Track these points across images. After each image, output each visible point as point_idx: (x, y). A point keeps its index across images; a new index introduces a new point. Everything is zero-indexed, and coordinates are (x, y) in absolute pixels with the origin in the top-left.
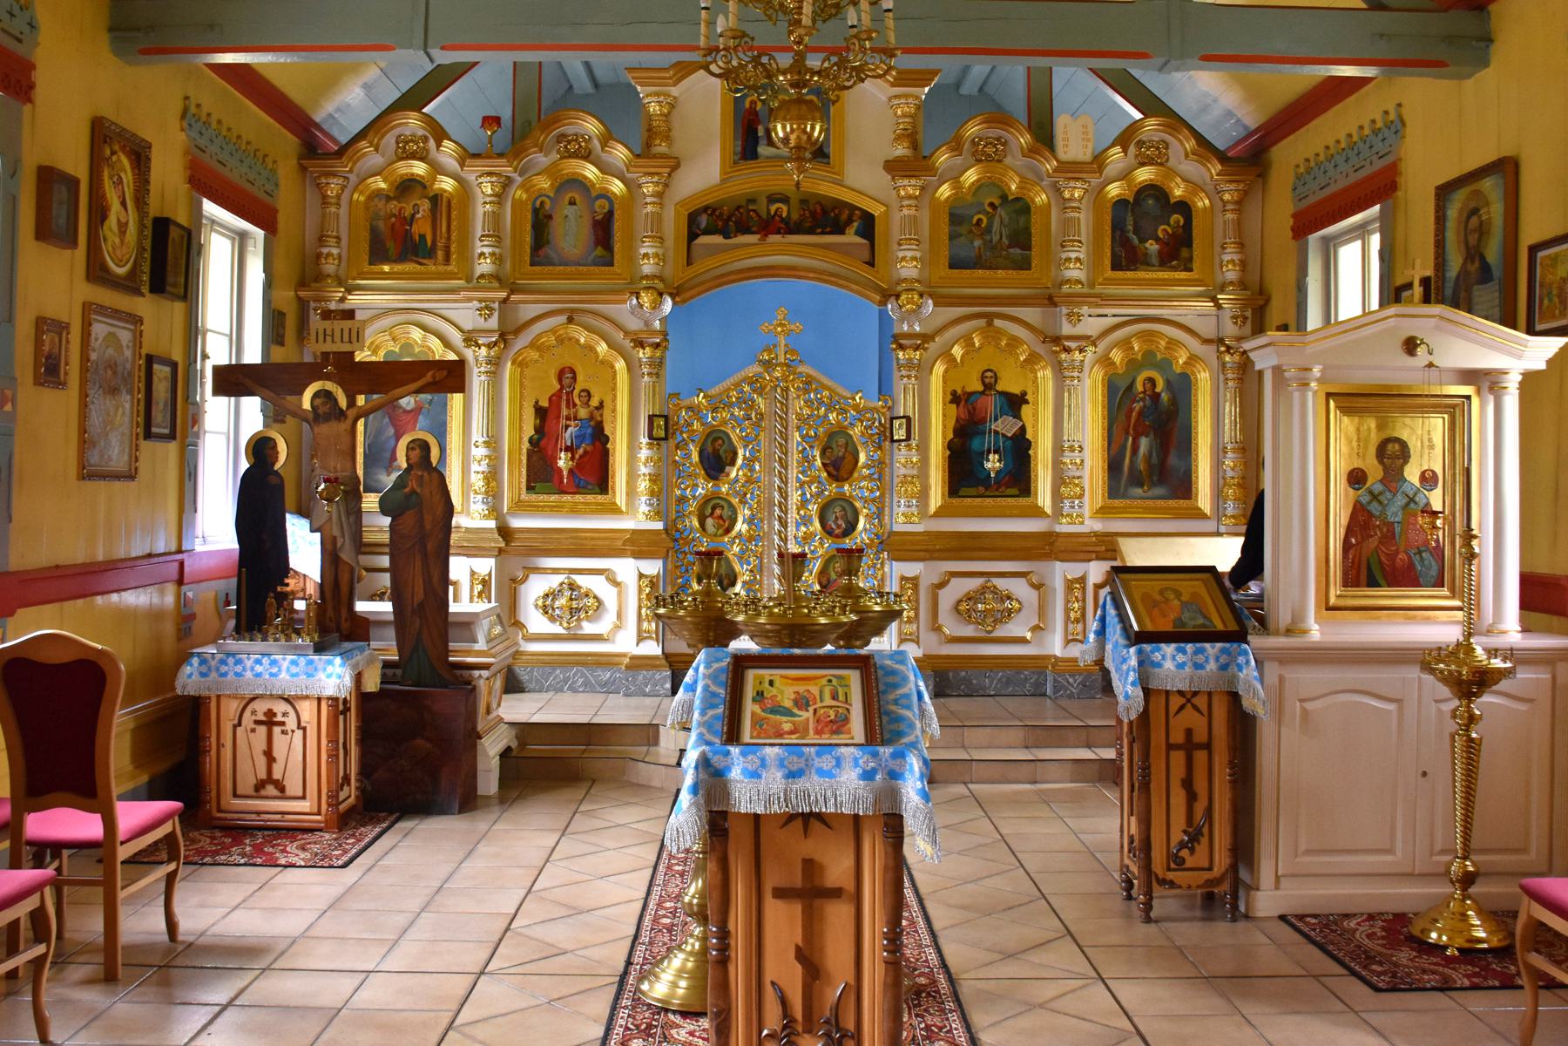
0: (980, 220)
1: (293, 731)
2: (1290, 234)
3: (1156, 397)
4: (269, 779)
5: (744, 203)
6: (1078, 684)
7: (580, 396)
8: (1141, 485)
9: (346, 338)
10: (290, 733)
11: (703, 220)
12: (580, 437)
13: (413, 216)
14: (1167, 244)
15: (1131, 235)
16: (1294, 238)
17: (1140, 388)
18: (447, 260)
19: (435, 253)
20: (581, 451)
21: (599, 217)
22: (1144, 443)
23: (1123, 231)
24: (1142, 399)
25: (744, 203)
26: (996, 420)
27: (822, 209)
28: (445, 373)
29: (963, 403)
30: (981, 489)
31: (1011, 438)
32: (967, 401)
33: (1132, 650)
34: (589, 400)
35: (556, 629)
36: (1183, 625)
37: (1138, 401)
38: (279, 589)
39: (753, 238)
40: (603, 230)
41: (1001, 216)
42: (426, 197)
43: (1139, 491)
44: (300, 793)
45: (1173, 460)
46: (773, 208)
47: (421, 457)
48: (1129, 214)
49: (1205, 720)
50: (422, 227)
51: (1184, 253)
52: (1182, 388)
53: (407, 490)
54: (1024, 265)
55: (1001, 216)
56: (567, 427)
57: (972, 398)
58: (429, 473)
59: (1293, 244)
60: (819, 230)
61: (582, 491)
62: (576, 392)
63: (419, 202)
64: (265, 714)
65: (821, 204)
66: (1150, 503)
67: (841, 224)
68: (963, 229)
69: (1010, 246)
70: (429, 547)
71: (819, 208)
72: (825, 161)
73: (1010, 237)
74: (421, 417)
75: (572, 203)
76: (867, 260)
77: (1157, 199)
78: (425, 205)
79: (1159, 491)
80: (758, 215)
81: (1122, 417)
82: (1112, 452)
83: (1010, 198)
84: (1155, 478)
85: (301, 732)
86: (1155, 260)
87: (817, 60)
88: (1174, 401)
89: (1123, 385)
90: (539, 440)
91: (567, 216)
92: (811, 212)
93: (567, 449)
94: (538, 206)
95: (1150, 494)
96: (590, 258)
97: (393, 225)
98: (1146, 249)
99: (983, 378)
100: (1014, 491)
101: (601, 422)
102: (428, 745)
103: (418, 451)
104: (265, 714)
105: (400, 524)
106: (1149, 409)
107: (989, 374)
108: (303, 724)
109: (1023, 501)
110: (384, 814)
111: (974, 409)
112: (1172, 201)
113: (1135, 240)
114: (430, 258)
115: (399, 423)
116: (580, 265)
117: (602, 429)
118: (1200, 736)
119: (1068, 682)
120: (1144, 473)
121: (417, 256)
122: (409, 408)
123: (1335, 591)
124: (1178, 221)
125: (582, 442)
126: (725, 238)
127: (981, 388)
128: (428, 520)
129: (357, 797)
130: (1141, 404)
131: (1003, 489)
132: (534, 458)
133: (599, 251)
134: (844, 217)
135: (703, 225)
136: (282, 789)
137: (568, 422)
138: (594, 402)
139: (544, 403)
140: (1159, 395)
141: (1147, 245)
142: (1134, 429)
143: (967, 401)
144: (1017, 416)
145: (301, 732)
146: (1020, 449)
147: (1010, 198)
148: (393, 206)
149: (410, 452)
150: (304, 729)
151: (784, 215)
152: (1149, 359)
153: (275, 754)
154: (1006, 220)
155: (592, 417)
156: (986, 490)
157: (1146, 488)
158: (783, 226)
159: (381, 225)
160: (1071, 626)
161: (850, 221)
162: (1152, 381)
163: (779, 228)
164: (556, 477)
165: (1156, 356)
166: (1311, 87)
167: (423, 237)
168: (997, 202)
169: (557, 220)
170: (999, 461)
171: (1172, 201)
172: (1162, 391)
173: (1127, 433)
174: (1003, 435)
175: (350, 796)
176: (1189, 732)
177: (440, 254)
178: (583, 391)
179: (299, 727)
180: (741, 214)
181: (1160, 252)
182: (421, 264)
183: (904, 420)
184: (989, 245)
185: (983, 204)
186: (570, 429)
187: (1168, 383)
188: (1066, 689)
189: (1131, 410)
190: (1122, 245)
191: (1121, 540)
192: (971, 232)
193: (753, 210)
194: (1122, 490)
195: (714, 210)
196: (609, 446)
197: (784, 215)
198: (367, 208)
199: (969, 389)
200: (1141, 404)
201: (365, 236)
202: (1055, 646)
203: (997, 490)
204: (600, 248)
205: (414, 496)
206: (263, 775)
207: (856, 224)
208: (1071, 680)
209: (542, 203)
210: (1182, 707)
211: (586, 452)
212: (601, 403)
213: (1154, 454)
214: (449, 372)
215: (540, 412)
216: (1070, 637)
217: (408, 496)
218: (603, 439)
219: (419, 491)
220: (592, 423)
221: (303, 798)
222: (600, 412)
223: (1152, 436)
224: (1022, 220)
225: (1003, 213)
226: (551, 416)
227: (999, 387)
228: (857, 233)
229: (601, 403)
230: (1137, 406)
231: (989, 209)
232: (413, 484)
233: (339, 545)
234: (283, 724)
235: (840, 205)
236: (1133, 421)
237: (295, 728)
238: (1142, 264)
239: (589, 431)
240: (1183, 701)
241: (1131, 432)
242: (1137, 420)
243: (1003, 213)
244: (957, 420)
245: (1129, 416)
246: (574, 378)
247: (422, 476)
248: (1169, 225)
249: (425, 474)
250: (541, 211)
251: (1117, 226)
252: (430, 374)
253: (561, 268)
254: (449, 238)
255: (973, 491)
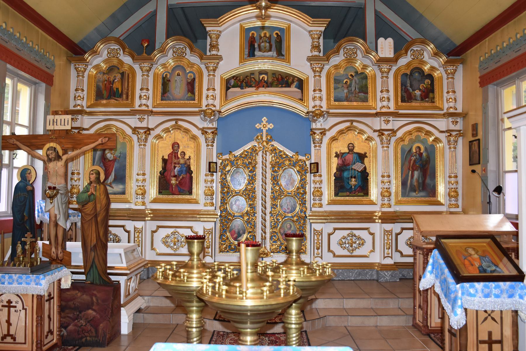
0: (346, 82)
1: (20, 311)
2: (478, 85)
3: (421, 154)
4: (9, 335)
5: (249, 75)
6: (390, 275)
7: (181, 154)
8: (415, 191)
9: (63, 123)
10: (19, 311)
11: (232, 82)
12: (180, 172)
13: (114, 81)
14: (424, 92)
15: (409, 88)
16: (480, 87)
17: (414, 151)
18: (127, 98)
19: (122, 96)
20: (181, 177)
21: (189, 81)
22: (416, 174)
23: (406, 87)
24: (415, 155)
25: (249, 75)
26: (354, 164)
27: (282, 77)
28: (107, 139)
29: (340, 157)
30: (348, 193)
31: (360, 172)
32: (342, 156)
33: (458, 286)
34: (185, 156)
35: (169, 251)
36: (485, 271)
37: (414, 156)
38: (23, 239)
39: (253, 89)
40: (191, 86)
41: (355, 80)
42: (119, 73)
43: (414, 194)
44: (24, 342)
45: (428, 181)
46: (261, 77)
47: (96, 178)
48: (408, 79)
49: (499, 326)
50: (117, 85)
51: (431, 95)
52: (431, 150)
53: (89, 193)
54: (366, 100)
55: (355, 80)
56: (175, 167)
57: (344, 155)
58: (99, 185)
59: (480, 90)
60: (280, 86)
61: (181, 193)
62: (179, 153)
63: (116, 75)
64: (7, 302)
65: (280, 75)
66: (419, 199)
67: (289, 83)
68: (340, 86)
69: (359, 92)
70: (99, 219)
71: (280, 77)
72: (283, 57)
73: (359, 89)
74: (116, 163)
75: (178, 75)
76: (300, 98)
77: (419, 73)
78: (119, 76)
79: (422, 194)
80: (255, 79)
81: (407, 163)
82: (403, 177)
83: (359, 73)
84: (421, 188)
85: (24, 311)
86: (419, 98)
87: (291, 154)
88: (428, 157)
89: (407, 149)
90: (164, 172)
91: (176, 80)
92: (277, 78)
93: (175, 176)
94: (164, 76)
95: (418, 195)
96: (185, 98)
97: (106, 84)
98: (415, 93)
99: (348, 147)
100: (362, 194)
101: (190, 165)
102: (94, 313)
103: (94, 175)
104: (7, 302)
105: (86, 209)
106: (418, 159)
107: (351, 145)
108: (25, 307)
109: (364, 199)
110: (70, 348)
111: (345, 160)
112: (426, 74)
113: (411, 90)
114: (120, 98)
115: (106, 165)
116: (181, 100)
117: (190, 168)
118: (496, 337)
119: (385, 275)
120: (416, 186)
121: (115, 97)
122: (111, 159)
123: (400, 103)
124: (428, 82)
125: (181, 174)
126: (241, 89)
127: (347, 151)
128: (98, 206)
129: (58, 339)
130: (415, 157)
131: (357, 193)
132: (162, 180)
133: (189, 94)
134: (290, 81)
135: (232, 84)
136: (14, 339)
137: (176, 165)
138: (187, 157)
139: (166, 157)
140: (422, 154)
141: (416, 92)
142: (412, 168)
143: (342, 156)
144: (363, 163)
145: (24, 311)
146: (364, 176)
147: (359, 73)
148: (106, 77)
149: (91, 175)
150: (26, 309)
151: (266, 79)
152: (418, 139)
153: (11, 322)
154: (357, 82)
155: (185, 163)
156: (350, 193)
157: (417, 192)
158: (265, 84)
159: (101, 84)
160: (386, 251)
161: (293, 82)
162: (419, 148)
163: (264, 85)
164: (171, 189)
165: (421, 138)
166: (489, 22)
167: (117, 89)
168: (353, 74)
169: (172, 81)
170: (356, 181)
171: (426, 74)
172: (423, 152)
173: (409, 169)
174: (357, 171)
175: (53, 339)
176: (490, 334)
177: (124, 96)
178: (182, 152)
179: (23, 309)
180: (248, 79)
181: (421, 95)
182: (116, 100)
183: (316, 164)
184: (350, 92)
185: (348, 75)
186: (177, 168)
187: (426, 149)
188: (384, 277)
189: (411, 160)
190: (405, 92)
191: (415, 216)
192: (343, 86)
193: (253, 78)
194: (407, 194)
195: (237, 78)
196: (192, 175)
197: (266, 79)
198: (95, 78)
199: (342, 151)
200: (415, 157)
201: (94, 89)
202: (376, 258)
203: (354, 193)
204: (189, 93)
205: (92, 196)
206: (5, 332)
207: (295, 83)
208: (386, 274)
209: (166, 75)
210: (486, 319)
211: (183, 178)
212: (190, 157)
213: (420, 179)
214: (109, 139)
215: (164, 161)
216: (386, 255)
217: (89, 196)
218: (190, 172)
219: (94, 193)
220: (186, 166)
221: (25, 343)
222: (189, 161)
223: (419, 171)
224: (364, 81)
225: (356, 79)
226: (168, 163)
227: (355, 151)
228: (296, 87)
229: (190, 157)
230: (413, 158)
231: (350, 77)
232: (92, 190)
233: (58, 218)
234: (15, 307)
235: (289, 76)
236: (411, 164)
237: (21, 309)
238: (414, 100)
239: (185, 169)
240: (487, 315)
241: (411, 169)
242: (413, 164)
243: (356, 79)
244: (338, 164)
245: (410, 163)
246: (179, 147)
247: (96, 186)
248: (425, 84)
249: (98, 186)
250: (166, 78)
251: (403, 84)
252: (100, 140)
253: (174, 101)
254: (128, 90)
255: (345, 194)
